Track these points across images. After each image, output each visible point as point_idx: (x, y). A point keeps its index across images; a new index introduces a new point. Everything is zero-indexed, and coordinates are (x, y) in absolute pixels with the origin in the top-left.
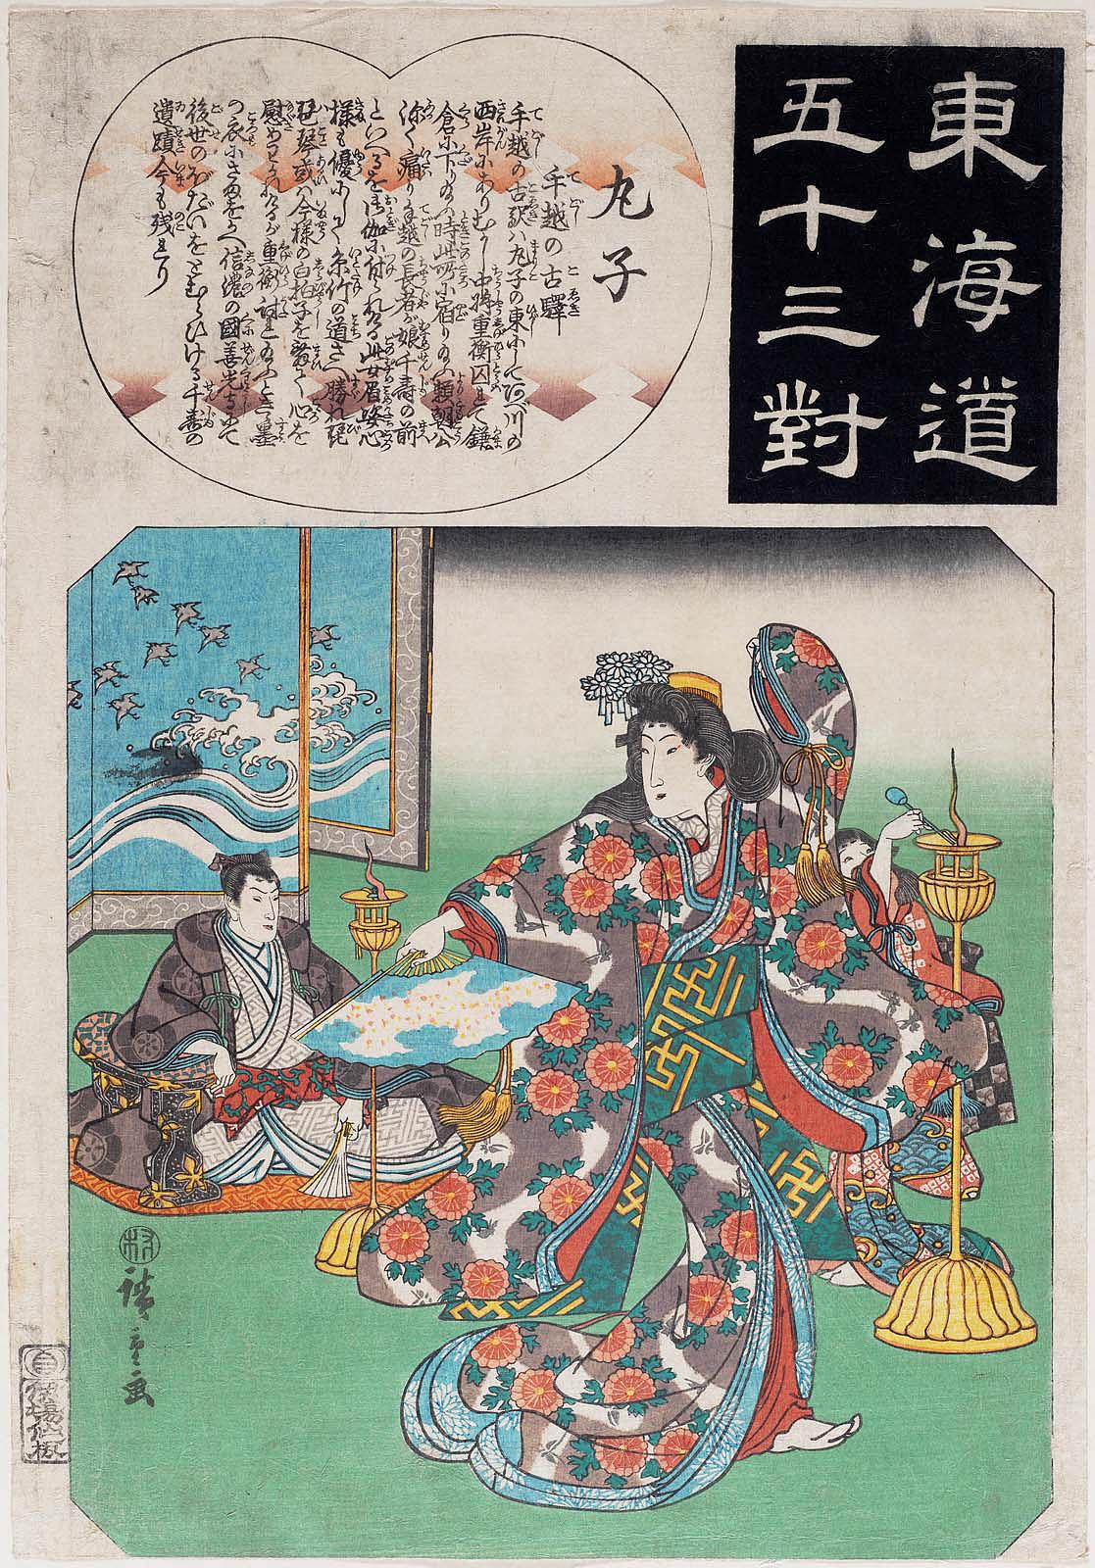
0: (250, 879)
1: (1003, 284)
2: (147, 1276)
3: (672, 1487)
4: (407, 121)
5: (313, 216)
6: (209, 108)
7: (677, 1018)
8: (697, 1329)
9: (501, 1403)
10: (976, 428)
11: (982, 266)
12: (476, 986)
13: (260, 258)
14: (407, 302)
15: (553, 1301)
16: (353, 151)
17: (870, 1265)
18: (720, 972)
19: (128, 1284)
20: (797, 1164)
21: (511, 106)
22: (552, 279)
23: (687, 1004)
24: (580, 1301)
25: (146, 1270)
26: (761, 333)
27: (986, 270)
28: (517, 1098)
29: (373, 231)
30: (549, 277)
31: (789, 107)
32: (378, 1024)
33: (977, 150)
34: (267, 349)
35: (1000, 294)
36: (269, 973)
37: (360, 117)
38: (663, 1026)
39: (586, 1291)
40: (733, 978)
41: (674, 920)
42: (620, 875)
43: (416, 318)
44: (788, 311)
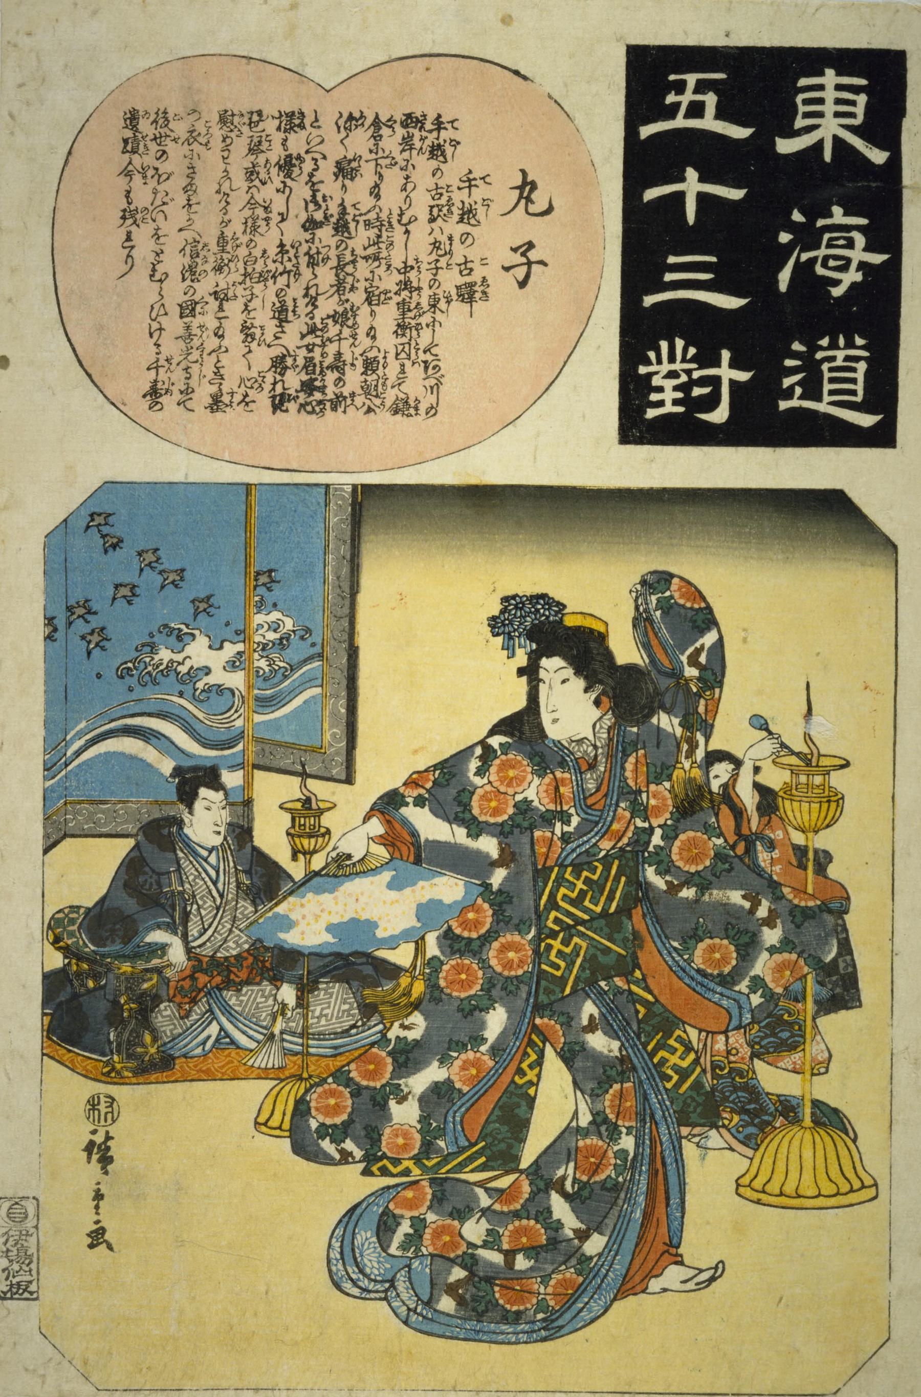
0: (203, 792)
1: (858, 255)
2: (108, 1138)
3: (560, 1322)
4: (342, 129)
5: (260, 212)
6: (170, 116)
7: (569, 914)
8: (584, 1186)
9: (413, 1249)
10: (832, 380)
11: (837, 239)
12: (394, 885)
13: (214, 247)
14: (339, 287)
15: (460, 1159)
16: (295, 155)
17: (733, 1131)
18: (605, 873)
19: (91, 1144)
20: (671, 1042)
21: (431, 117)
22: (466, 267)
23: (577, 902)
24: (483, 1159)
25: (107, 1132)
26: (648, 410)
27: (841, 242)
28: (433, 986)
29: (311, 225)
30: (463, 267)
31: (671, 98)
32: (310, 918)
33: (835, 138)
34: (219, 328)
35: (854, 265)
36: (218, 872)
37: (302, 126)
38: (557, 921)
39: (488, 1152)
40: (617, 879)
41: (566, 829)
42: (520, 789)
43: (347, 301)
44: (669, 277)
